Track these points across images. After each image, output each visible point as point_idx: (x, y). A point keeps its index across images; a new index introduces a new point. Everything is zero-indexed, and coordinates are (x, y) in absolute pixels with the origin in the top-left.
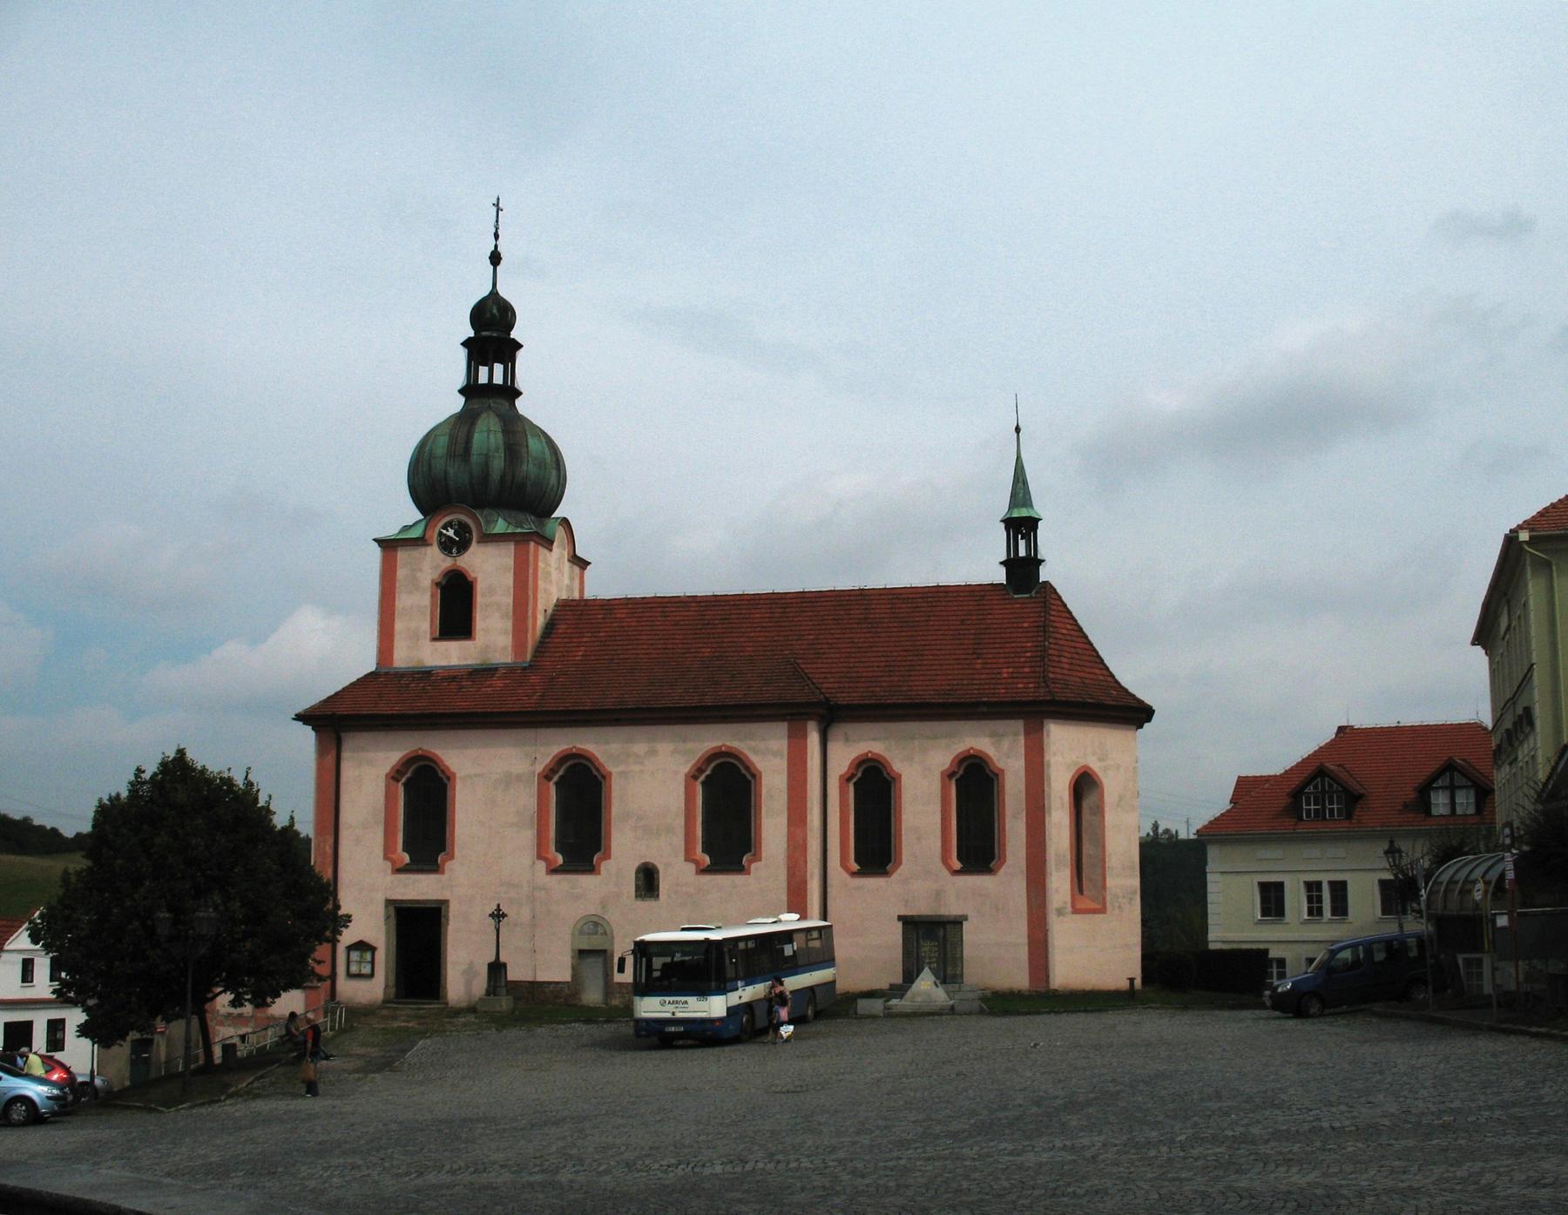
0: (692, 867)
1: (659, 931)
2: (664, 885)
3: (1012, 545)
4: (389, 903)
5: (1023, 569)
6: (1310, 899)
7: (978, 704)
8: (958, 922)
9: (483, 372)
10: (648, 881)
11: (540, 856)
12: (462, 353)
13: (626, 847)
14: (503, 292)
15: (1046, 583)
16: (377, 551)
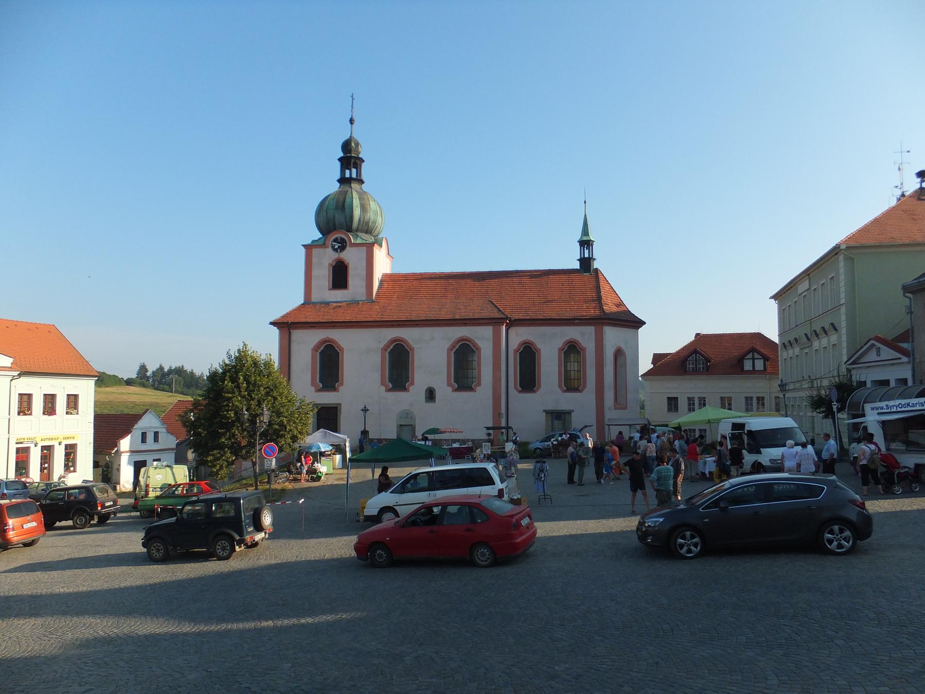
0: (450, 389)
1: (152, 640)
2: (438, 396)
3: (582, 252)
4: (340, 404)
5: (586, 263)
6: (689, 404)
7: (574, 319)
8: (569, 413)
9: (347, 172)
10: (431, 395)
11: (382, 384)
12: (338, 164)
13: (421, 379)
14: (355, 136)
15: (597, 269)
16: (303, 250)
